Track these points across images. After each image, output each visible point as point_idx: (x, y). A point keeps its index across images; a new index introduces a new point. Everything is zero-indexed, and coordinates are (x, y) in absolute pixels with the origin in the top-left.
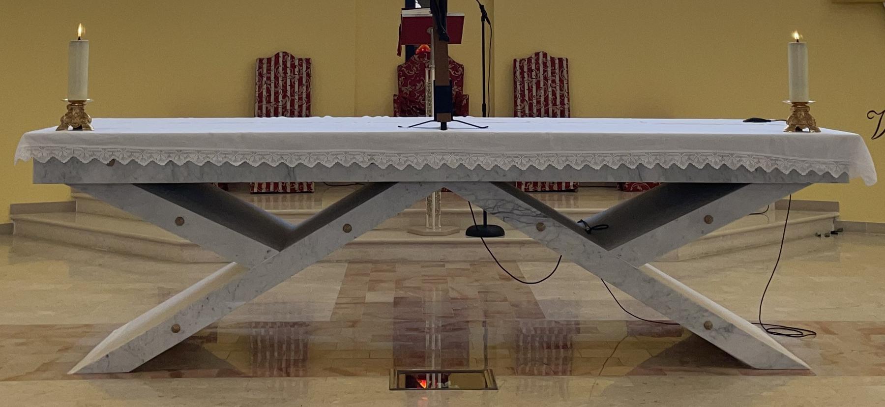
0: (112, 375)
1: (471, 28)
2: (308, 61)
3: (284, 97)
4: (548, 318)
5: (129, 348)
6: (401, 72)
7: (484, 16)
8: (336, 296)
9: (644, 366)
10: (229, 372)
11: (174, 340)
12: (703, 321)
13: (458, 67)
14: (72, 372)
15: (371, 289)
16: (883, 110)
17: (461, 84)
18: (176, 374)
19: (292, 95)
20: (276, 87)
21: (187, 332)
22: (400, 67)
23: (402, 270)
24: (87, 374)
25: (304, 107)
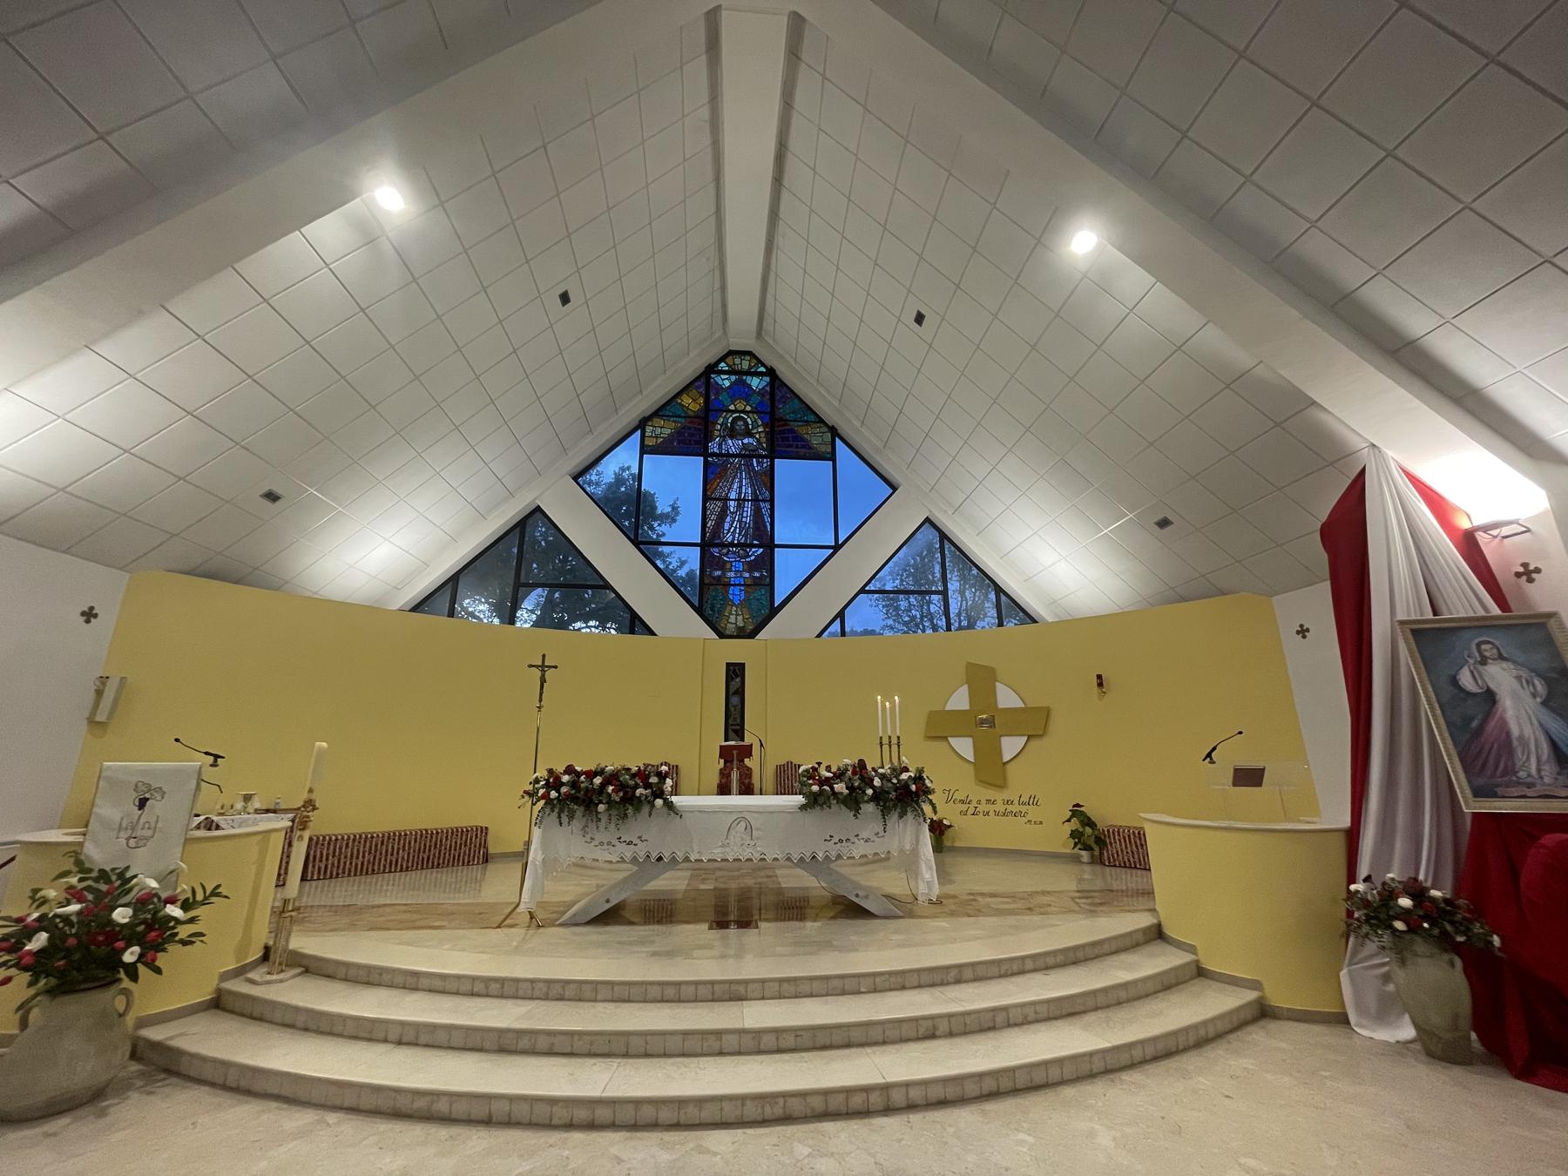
0: (576, 925)
1: (756, 750)
2: (677, 766)
3: (370, 853)
4: (786, 896)
5: (584, 910)
6: (721, 771)
7: (762, 745)
8: (686, 882)
9: (841, 912)
10: (631, 923)
11: (608, 906)
12: (855, 893)
13: (749, 769)
14: (557, 923)
15: (702, 883)
16: (4, 987)
17: (750, 777)
18: (607, 924)
19: (376, 851)
20: (364, 847)
21: (614, 902)
22: (721, 770)
23: (719, 874)
24: (561, 925)
25: (348, 863)
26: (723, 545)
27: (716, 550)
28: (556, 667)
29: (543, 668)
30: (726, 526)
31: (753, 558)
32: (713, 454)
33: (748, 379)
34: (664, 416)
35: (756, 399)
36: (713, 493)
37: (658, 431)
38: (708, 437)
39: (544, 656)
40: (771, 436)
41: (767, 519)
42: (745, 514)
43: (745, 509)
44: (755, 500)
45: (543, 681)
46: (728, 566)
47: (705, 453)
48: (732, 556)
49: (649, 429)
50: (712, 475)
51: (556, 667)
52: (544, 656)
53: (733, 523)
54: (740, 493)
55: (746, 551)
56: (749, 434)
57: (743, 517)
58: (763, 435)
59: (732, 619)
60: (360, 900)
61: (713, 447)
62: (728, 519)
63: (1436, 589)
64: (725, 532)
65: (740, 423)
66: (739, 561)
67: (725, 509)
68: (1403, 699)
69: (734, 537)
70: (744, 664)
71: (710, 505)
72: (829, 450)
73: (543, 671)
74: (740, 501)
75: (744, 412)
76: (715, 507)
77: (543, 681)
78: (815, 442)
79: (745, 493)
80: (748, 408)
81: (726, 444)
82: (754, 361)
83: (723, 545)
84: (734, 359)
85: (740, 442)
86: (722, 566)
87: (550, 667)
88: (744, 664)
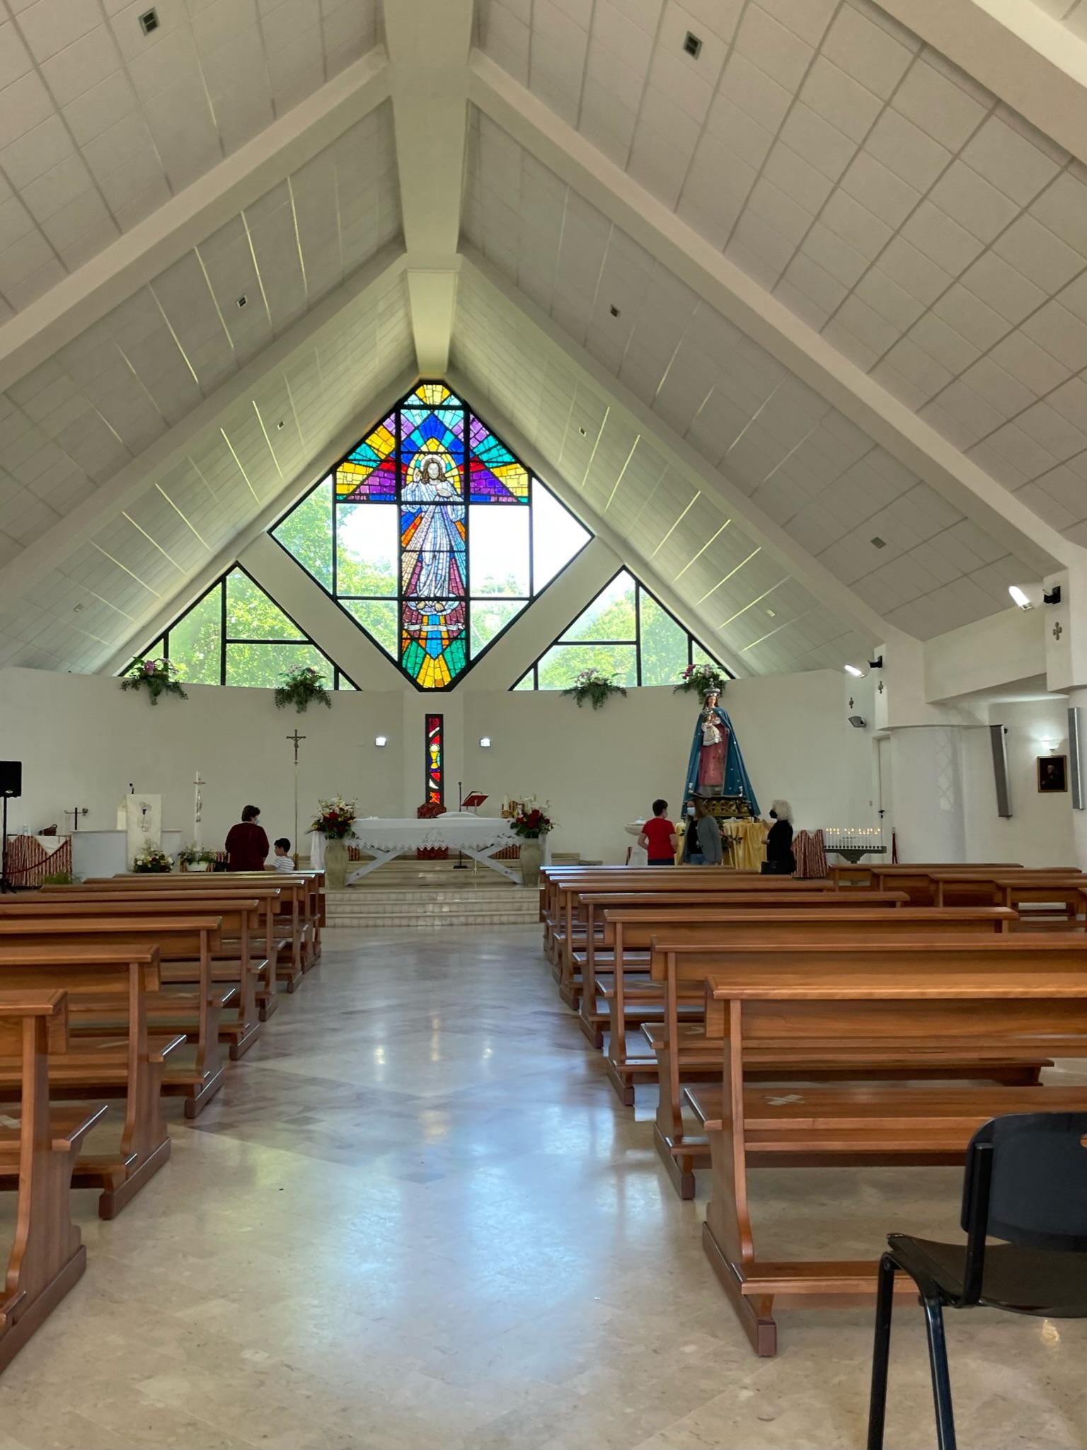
26: (419, 599)
27: (413, 603)
28: (304, 737)
29: (296, 738)
30: (423, 579)
31: (449, 611)
32: (406, 503)
33: (440, 414)
34: (355, 460)
35: (449, 438)
36: (408, 544)
37: (349, 477)
38: (400, 483)
39: (296, 731)
40: (466, 481)
41: (463, 571)
42: (440, 567)
43: (441, 561)
44: (451, 551)
45: (296, 746)
46: (425, 619)
47: (399, 503)
48: (429, 609)
49: (339, 475)
50: (407, 523)
51: (304, 737)
52: (296, 731)
53: (429, 575)
54: (435, 544)
55: (442, 604)
56: (442, 477)
57: (438, 569)
58: (457, 479)
59: (430, 672)
60: (827, 898)
61: (406, 494)
62: (424, 572)
63: (814, 1065)
64: (422, 585)
65: (433, 466)
66: (435, 615)
67: (420, 560)
68: (810, 1056)
69: (430, 590)
70: (442, 715)
71: (405, 557)
72: (526, 493)
73: (296, 741)
74: (435, 552)
75: (436, 453)
76: (410, 559)
77: (296, 746)
78: (510, 484)
79: (440, 544)
80: (442, 449)
81: (419, 490)
82: (447, 392)
83: (419, 599)
84: (474, 448)
85: (831, 830)
86: (419, 619)
87: (301, 738)
88: (442, 715)
